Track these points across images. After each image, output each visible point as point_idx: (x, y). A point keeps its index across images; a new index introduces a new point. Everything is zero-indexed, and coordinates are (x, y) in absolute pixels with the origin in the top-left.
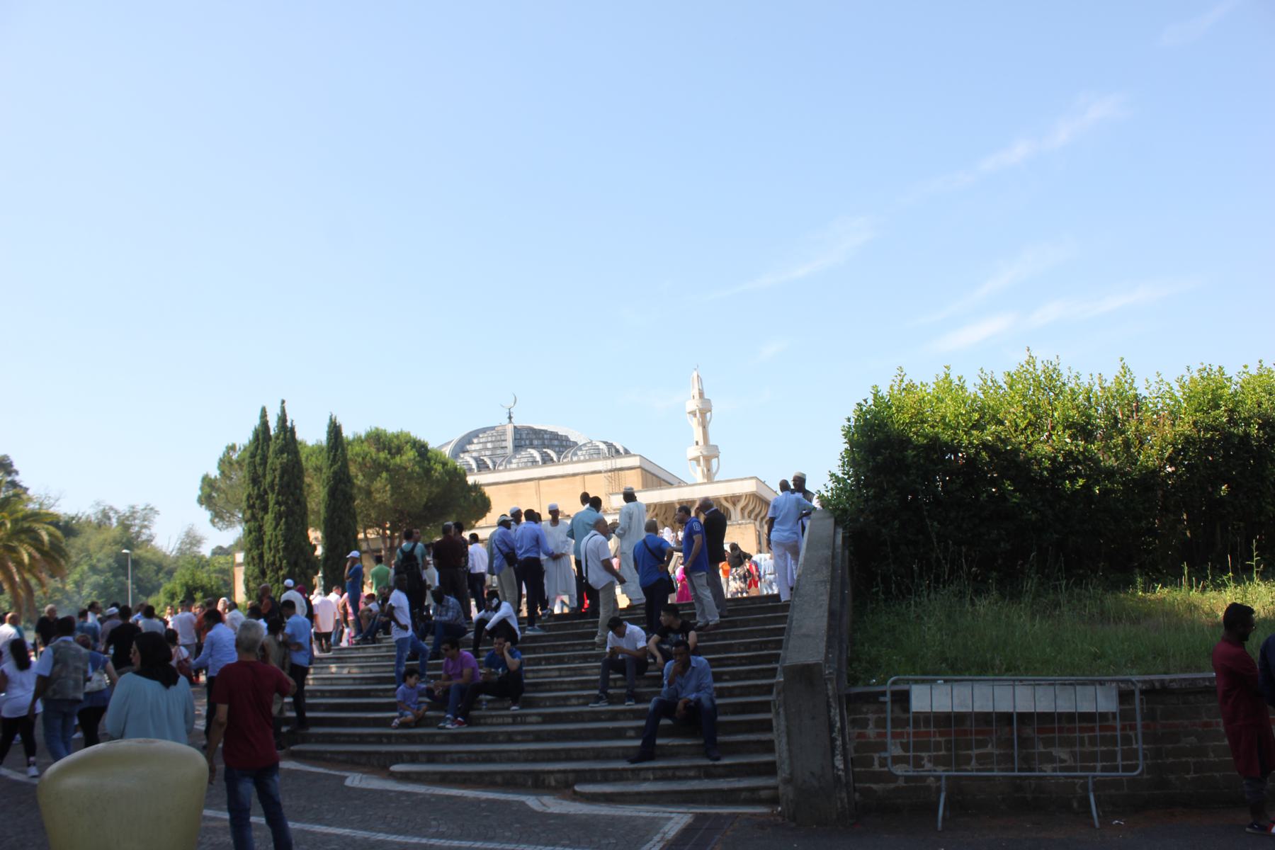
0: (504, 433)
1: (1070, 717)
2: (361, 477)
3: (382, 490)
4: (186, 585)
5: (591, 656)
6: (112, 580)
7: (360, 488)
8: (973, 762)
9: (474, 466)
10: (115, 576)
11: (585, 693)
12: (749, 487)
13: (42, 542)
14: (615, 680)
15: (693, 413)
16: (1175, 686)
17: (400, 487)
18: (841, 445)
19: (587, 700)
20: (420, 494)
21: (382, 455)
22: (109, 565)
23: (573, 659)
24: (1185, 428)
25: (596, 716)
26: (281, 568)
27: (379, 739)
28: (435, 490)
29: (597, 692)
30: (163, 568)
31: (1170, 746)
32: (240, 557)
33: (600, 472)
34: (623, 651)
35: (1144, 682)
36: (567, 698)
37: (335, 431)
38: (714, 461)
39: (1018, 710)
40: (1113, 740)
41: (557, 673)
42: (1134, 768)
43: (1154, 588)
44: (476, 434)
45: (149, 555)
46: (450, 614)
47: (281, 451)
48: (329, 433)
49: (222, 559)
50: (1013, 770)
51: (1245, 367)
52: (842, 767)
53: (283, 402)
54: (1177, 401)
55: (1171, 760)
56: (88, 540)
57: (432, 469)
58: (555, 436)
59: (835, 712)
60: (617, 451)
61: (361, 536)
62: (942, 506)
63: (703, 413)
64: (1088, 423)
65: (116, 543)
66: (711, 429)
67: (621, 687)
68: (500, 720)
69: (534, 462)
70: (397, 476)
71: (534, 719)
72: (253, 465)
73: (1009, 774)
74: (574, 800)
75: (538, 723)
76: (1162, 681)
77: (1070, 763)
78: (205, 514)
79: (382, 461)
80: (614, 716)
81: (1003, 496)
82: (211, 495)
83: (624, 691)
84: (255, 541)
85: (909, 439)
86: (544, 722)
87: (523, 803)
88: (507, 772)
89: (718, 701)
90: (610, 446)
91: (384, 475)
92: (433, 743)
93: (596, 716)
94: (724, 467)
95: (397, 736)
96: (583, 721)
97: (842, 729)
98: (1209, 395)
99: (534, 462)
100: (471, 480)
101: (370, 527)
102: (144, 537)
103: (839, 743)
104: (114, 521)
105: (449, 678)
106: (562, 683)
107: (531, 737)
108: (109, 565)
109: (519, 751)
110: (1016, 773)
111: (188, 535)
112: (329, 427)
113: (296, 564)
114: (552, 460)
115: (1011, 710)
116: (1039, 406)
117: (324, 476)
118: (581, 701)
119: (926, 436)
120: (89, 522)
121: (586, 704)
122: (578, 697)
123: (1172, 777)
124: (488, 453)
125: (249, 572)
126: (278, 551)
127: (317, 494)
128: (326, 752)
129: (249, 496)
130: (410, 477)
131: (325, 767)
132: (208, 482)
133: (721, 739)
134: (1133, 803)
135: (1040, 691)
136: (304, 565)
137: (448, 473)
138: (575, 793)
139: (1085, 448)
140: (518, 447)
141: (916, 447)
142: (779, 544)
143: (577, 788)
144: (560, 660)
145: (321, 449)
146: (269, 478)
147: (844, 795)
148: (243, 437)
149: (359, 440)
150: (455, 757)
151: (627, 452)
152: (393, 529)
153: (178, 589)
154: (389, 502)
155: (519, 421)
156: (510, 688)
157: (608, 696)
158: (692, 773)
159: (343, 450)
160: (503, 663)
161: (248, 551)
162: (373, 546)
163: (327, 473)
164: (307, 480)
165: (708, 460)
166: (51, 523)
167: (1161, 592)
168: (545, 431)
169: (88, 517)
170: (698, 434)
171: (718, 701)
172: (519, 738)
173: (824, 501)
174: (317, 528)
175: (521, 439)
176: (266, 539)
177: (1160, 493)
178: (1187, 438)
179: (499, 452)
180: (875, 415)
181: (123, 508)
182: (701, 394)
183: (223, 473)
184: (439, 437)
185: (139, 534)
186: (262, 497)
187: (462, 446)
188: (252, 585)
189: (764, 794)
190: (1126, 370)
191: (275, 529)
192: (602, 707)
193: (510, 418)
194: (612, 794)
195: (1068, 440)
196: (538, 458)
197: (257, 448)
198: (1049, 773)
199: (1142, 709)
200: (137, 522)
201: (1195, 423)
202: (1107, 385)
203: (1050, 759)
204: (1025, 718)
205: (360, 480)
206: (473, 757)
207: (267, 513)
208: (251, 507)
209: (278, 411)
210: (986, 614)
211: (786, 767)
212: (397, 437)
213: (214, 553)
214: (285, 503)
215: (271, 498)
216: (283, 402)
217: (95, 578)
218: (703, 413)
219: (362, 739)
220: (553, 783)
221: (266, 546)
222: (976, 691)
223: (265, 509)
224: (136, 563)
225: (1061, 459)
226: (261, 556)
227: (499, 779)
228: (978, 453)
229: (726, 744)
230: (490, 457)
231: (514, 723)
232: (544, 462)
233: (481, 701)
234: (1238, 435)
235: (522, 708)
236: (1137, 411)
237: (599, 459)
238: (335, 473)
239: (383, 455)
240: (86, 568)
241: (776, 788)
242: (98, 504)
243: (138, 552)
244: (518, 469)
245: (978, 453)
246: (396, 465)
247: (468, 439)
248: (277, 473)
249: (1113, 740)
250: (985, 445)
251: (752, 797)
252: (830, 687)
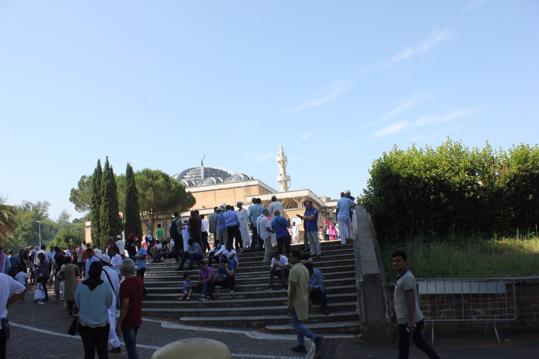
0: (200, 170)
1: (485, 295)
2: (140, 189)
3: (150, 195)
4: (65, 236)
5: (262, 268)
6: (31, 233)
7: (140, 194)
8: (442, 315)
9: (187, 184)
10: (32, 232)
11: (263, 285)
12: (305, 194)
13: (5, 218)
14: (275, 279)
15: (279, 162)
16: (528, 282)
17: (157, 194)
18: (370, 177)
19: (264, 288)
20: (166, 197)
21: (149, 180)
22: (30, 227)
23: (253, 270)
24: (514, 170)
25: (269, 295)
26: (107, 229)
27: (172, 306)
28: (172, 195)
29: (268, 284)
30: (53, 228)
31: (525, 307)
32: (88, 223)
33: (241, 187)
34: (278, 266)
35: (515, 280)
36: (255, 287)
37: (129, 169)
38: (288, 182)
39: (464, 293)
40: (503, 305)
41: (247, 276)
42: (513, 317)
43: (502, 239)
44: (188, 171)
45: (47, 223)
46: (196, 250)
47: (107, 178)
48: (127, 171)
49: (78, 224)
50: (462, 318)
51: (536, 145)
52: (388, 318)
53: (107, 157)
54: (508, 159)
55: (526, 313)
56: (20, 217)
57: (171, 186)
58: (221, 172)
59: (385, 294)
60: (248, 178)
61: (141, 214)
62: (413, 203)
63: (284, 162)
64: (475, 169)
65: (33, 218)
66: (287, 169)
67: (277, 282)
68: (226, 297)
69: (213, 183)
70: (156, 188)
71: (241, 296)
72: (94, 184)
73: (459, 320)
74: (267, 333)
75: (243, 298)
76: (523, 280)
77: (484, 315)
78: (73, 205)
79: (150, 182)
80: (277, 295)
81: (439, 199)
82: (75, 197)
83: (280, 284)
84: (95, 217)
85: (400, 175)
86: (246, 298)
87: (244, 334)
88: (234, 320)
89: (326, 288)
90: (245, 176)
91: (151, 188)
92: (197, 307)
93: (269, 295)
94: (292, 185)
95: (181, 304)
96: (263, 297)
97: (388, 302)
98: (523, 157)
99: (213, 183)
100: (187, 190)
101: (145, 211)
102: (44, 215)
103: (387, 307)
104: (31, 208)
105: (202, 279)
106: (251, 280)
107: (242, 305)
108: (30, 227)
109: (238, 311)
110: (463, 320)
111: (63, 214)
112: (127, 168)
113: (114, 227)
114: (220, 182)
115: (461, 293)
116: (453, 161)
117: (125, 189)
118: (261, 288)
119: (407, 174)
120: (20, 209)
121: (264, 290)
122: (260, 287)
123: (526, 320)
124: (193, 179)
125: (93, 231)
127: (122, 196)
128: (150, 312)
129: (93, 198)
130: (162, 189)
131: (150, 319)
132: (73, 192)
133: (329, 305)
134: (511, 332)
135: (473, 284)
136: (117, 227)
137: (178, 187)
138: (266, 329)
139: (474, 179)
140: (206, 176)
141: (403, 178)
142: (340, 220)
143: (267, 327)
144: (248, 270)
145: (123, 177)
146: (102, 190)
147: (389, 330)
148: (90, 172)
149: (139, 173)
150: (209, 314)
151: (252, 178)
152: (154, 212)
153: (62, 238)
154: (152, 200)
155: (206, 166)
156: (229, 283)
157: (273, 286)
158: (317, 320)
159: (133, 178)
160: (226, 273)
161: (93, 222)
162: (145, 219)
163: (126, 188)
164: (118, 191)
165: (286, 182)
166: (10, 211)
167: (505, 241)
168: (217, 170)
169: (20, 206)
170: (281, 171)
171: (326, 288)
172: (236, 305)
173: (359, 201)
174: (121, 211)
175: (207, 173)
176: (101, 216)
177: (504, 198)
178: (515, 175)
179: (198, 178)
180: (385, 164)
181: (35, 203)
182: (283, 154)
183: (80, 188)
184: (173, 172)
185: (42, 214)
186: (98, 198)
187: (182, 176)
188: (95, 236)
189: (351, 329)
190: (489, 146)
191: (104, 212)
192: (271, 291)
193: (202, 164)
194: (284, 330)
195: (467, 176)
196: (215, 181)
197: (96, 177)
198: (475, 320)
199: (516, 292)
200: (41, 208)
201: (519, 168)
202: (479, 152)
203: (475, 313)
204: (467, 296)
205: (140, 191)
206: (217, 314)
207: (101, 205)
208: (94, 202)
209: (105, 161)
210: (438, 249)
211: (364, 318)
212: (156, 172)
213: (74, 221)
214: (109, 201)
215: (103, 199)
216: (107, 157)
217: (24, 233)
218: (284, 162)
219: (164, 306)
220: (255, 325)
221: (101, 219)
222: (446, 284)
223: (100, 203)
224: (42, 227)
225: (463, 183)
226: (98, 223)
227: (231, 324)
228: (429, 181)
229: (330, 307)
230: (194, 181)
231: (232, 299)
232: (217, 183)
233: (216, 289)
234: (536, 174)
235: (235, 291)
236: (494, 163)
237: (240, 182)
238: (130, 188)
239: (150, 180)
240: (20, 228)
241: (359, 326)
242: (24, 201)
243: (43, 221)
244: (206, 186)
245: (429, 181)
246: (155, 184)
247: (184, 173)
248: (105, 188)
249: (503, 305)
250: (432, 178)
251: (346, 331)
252: (383, 283)
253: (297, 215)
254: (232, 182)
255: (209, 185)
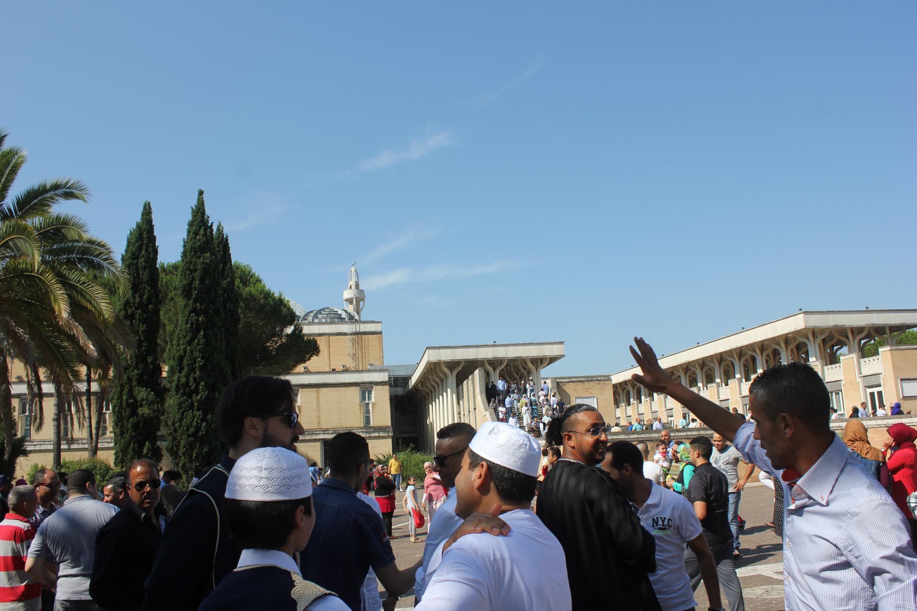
26: (197, 392)
33: (345, 334)
53: (201, 193)
126: (193, 370)
145: (175, 267)
182: (357, 286)
214: (205, 313)
216: (201, 193)
248: (197, 275)
253: (564, 356)
254: (321, 323)
255: (332, 323)
